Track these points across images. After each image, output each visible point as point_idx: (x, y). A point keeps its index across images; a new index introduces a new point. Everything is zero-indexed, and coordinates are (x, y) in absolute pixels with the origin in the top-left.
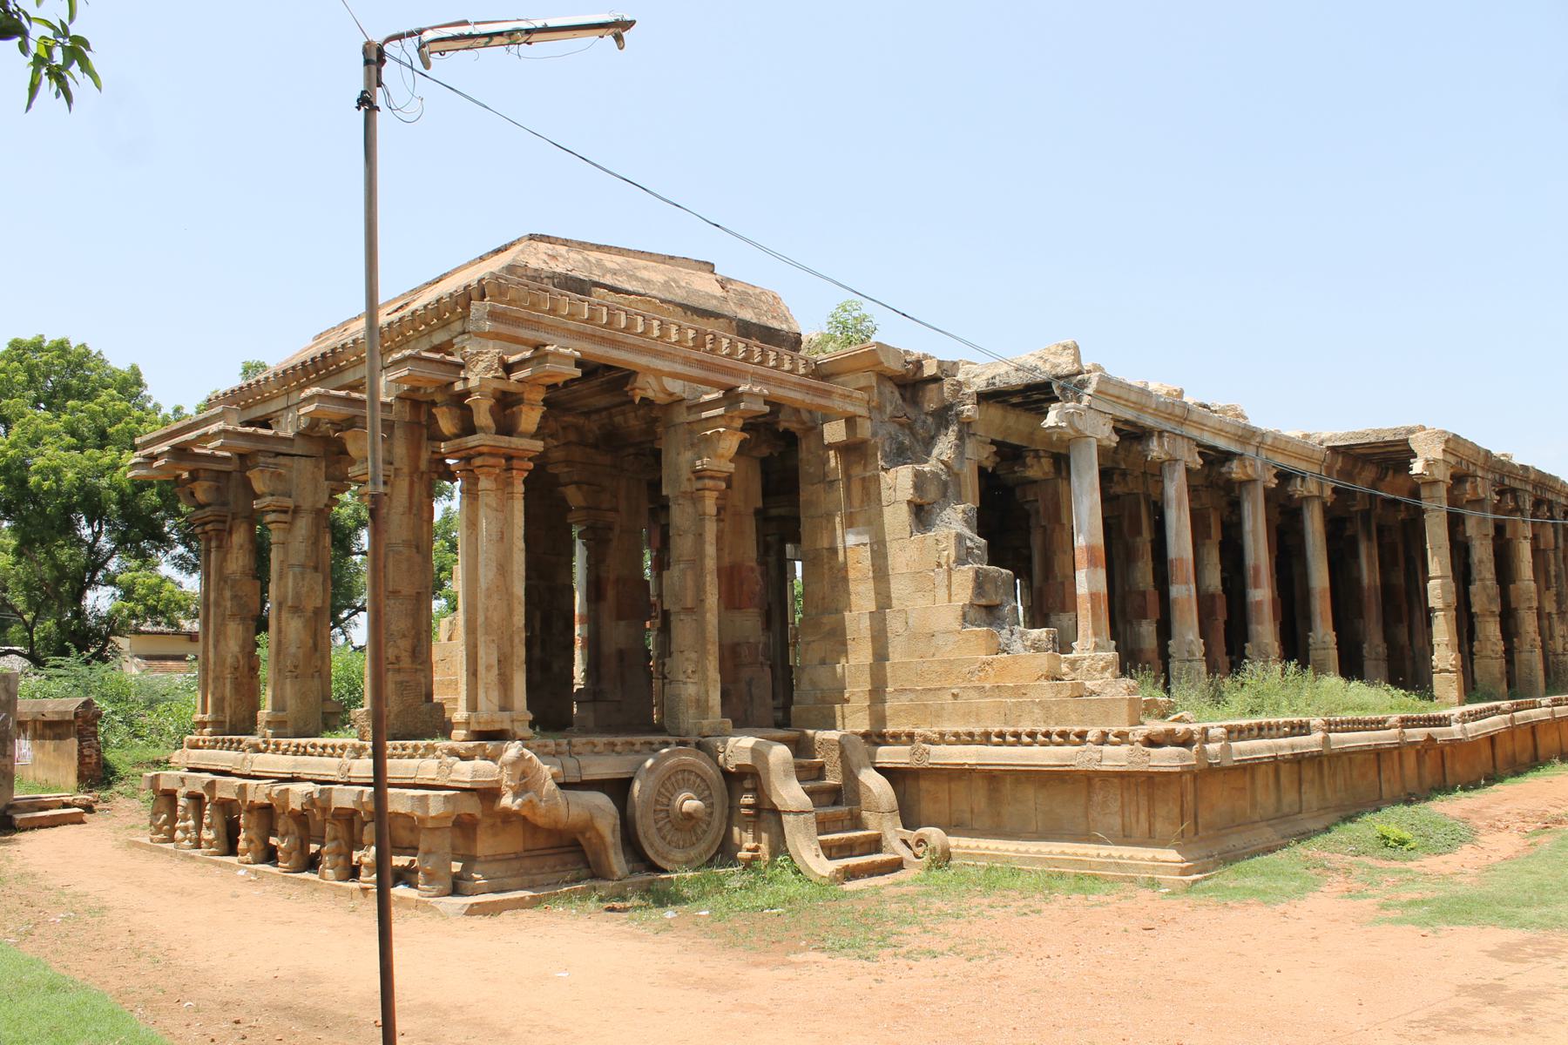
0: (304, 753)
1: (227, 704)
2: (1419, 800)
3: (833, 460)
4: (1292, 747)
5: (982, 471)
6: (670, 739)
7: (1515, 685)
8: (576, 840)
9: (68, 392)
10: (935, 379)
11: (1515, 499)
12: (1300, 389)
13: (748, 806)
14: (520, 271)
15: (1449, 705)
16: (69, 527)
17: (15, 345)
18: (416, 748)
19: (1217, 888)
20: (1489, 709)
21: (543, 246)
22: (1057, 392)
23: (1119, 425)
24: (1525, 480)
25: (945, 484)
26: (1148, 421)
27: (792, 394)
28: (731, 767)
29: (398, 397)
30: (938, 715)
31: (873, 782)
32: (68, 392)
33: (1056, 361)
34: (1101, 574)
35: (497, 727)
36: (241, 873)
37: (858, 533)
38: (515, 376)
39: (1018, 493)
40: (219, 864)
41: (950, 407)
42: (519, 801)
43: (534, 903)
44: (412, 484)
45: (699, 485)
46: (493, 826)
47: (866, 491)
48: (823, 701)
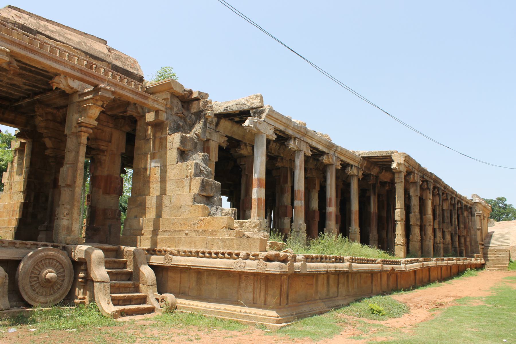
2: (387, 294)
3: (150, 131)
4: (335, 267)
5: (220, 148)
6: (48, 244)
7: (424, 253)
10: (197, 99)
11: (427, 184)
12: (352, 131)
13: (82, 278)
15: (401, 258)
19: (292, 331)
20: (415, 260)
22: (252, 114)
23: (277, 132)
24: (431, 178)
25: (196, 144)
26: (290, 132)
27: (127, 94)
30: (179, 242)
31: (147, 272)
33: (252, 102)
34: (263, 191)
37: (156, 162)
39: (238, 161)
41: (202, 111)
45: (79, 129)
47: (161, 143)
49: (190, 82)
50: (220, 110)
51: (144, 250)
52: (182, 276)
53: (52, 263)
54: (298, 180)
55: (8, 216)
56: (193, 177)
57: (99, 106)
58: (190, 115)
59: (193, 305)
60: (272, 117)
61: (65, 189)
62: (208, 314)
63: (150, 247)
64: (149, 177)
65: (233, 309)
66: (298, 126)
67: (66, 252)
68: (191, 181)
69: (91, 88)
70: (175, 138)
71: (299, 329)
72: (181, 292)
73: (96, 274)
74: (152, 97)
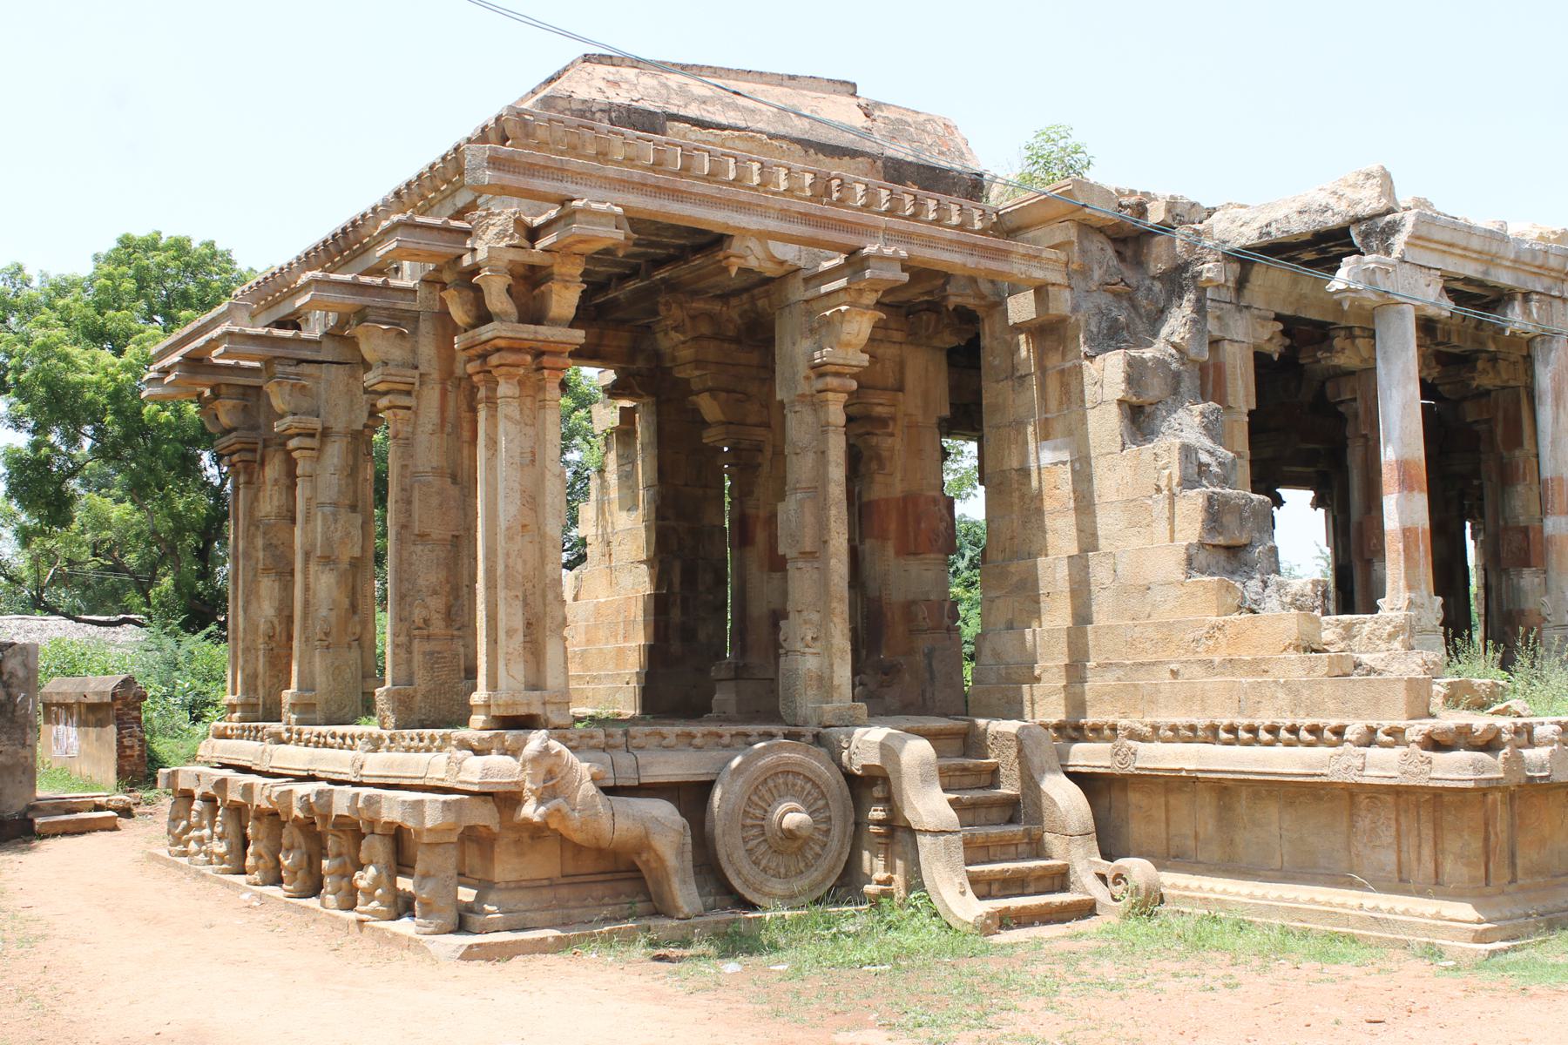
0: (325, 745)
1: (260, 682)
3: (1024, 349)
5: (1260, 359)
6: (773, 728)
8: (634, 863)
9: (185, 299)
10: (1165, 228)
13: (879, 823)
14: (561, 104)
16: (188, 466)
17: (126, 243)
18: (432, 738)
21: (602, 70)
22: (1357, 241)
23: (1459, 286)
25: (1177, 376)
26: (1504, 278)
27: (946, 256)
28: (856, 769)
29: (424, 281)
31: (1063, 795)
32: (185, 299)
33: (1356, 196)
34: (1421, 501)
35: (522, 711)
36: (246, 896)
37: (1055, 449)
38: (541, 244)
39: (1330, 389)
40: (227, 885)
41: (1183, 267)
42: (542, 809)
43: (560, 946)
44: (444, 394)
45: (820, 384)
46: (518, 842)
47: (1065, 387)
48: (1008, 679)
49: (1131, 165)
50: (1248, 236)
51: (1045, 726)
52: (1172, 801)
53: (794, 785)
54: (1553, 442)
55: (612, 640)
56: (1177, 490)
57: (867, 307)
58: (1148, 282)
59: (1212, 890)
60: (1430, 240)
61: (800, 565)
62: (1260, 915)
63: (1063, 717)
64: (1039, 496)
65: (1338, 900)
66: (1533, 251)
67: (823, 751)
68: (1172, 504)
69: (839, 260)
70: (1108, 369)
71: (1551, 961)
72: (1172, 853)
73: (920, 810)
74: (1019, 247)
